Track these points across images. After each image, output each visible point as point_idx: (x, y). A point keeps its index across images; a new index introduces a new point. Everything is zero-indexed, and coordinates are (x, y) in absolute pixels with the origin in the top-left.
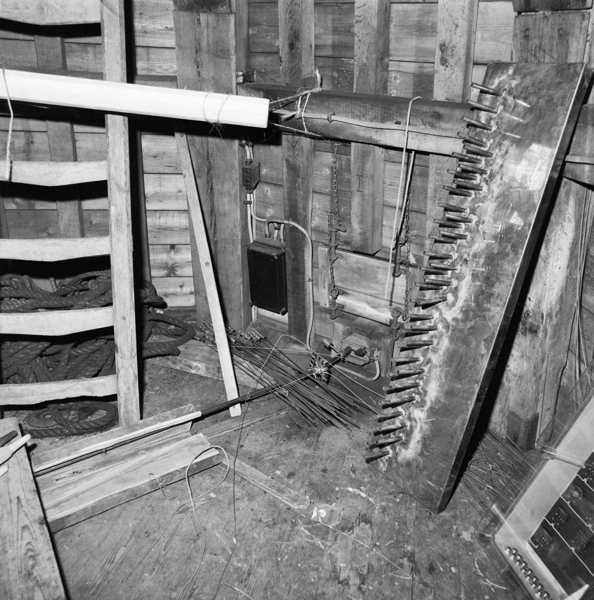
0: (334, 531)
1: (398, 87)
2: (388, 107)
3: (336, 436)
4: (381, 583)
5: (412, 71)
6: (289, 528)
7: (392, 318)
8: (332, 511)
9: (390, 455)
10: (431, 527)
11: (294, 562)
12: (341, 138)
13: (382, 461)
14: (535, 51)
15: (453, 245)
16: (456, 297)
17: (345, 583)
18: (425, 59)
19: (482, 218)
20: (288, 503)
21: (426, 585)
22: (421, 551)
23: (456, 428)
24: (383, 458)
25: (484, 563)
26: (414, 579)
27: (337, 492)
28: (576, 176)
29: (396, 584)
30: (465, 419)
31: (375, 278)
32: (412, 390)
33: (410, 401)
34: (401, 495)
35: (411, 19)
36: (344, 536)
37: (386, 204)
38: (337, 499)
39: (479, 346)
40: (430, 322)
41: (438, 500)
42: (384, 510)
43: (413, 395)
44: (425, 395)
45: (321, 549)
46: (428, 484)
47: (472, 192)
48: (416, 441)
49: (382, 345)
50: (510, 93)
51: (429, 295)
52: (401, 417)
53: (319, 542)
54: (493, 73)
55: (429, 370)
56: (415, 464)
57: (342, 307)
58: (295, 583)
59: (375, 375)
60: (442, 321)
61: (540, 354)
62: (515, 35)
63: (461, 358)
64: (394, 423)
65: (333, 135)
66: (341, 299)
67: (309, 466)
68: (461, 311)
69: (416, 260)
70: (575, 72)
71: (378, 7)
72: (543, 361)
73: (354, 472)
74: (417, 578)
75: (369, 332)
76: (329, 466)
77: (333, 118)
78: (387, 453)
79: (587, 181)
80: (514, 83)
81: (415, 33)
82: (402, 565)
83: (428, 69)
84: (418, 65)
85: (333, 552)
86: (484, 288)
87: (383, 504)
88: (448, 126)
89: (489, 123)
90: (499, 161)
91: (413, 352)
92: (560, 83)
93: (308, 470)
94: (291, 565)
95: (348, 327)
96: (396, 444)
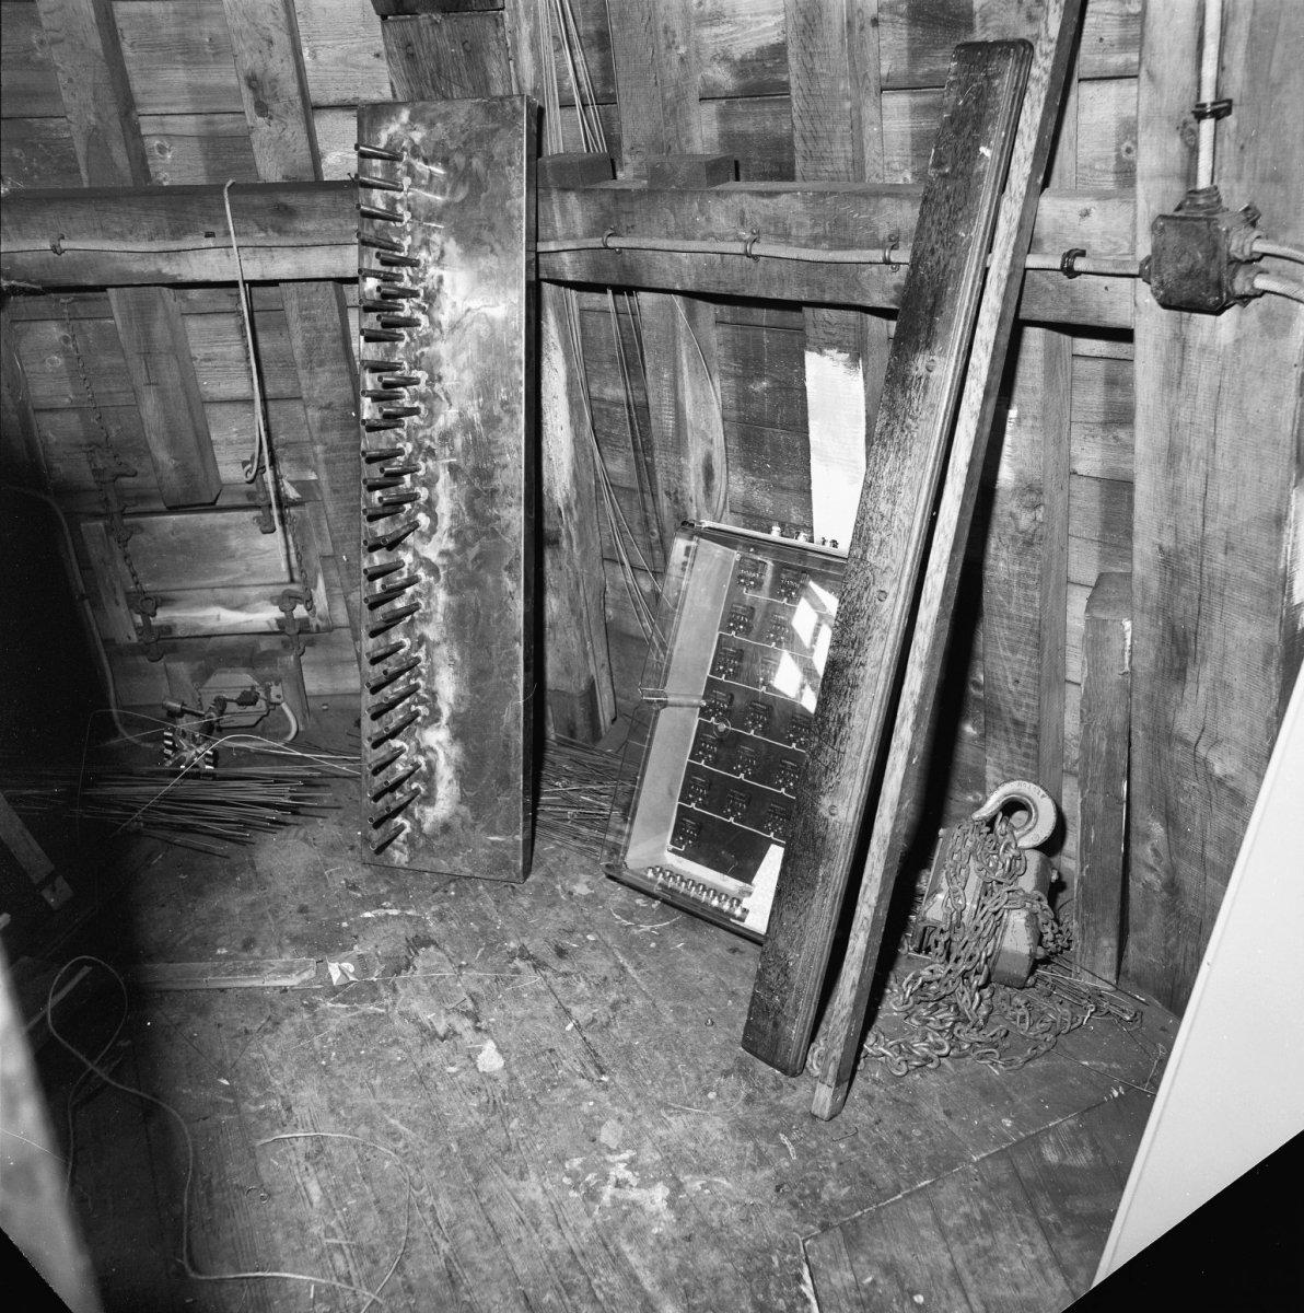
0: (385, 982)
1: (175, 165)
2: (185, 209)
3: (284, 853)
4: (503, 1007)
5: (193, 131)
6: (306, 1016)
7: (282, 615)
8: (361, 957)
9: (408, 830)
10: (526, 903)
11: (352, 1054)
12: (91, 283)
13: (396, 848)
14: (432, 80)
15: (398, 430)
16: (434, 517)
17: (451, 1034)
18: (215, 107)
19: (436, 372)
20: (278, 983)
21: (566, 974)
22: (531, 939)
23: (507, 728)
24: (395, 842)
25: (625, 908)
26: (545, 977)
27: (348, 929)
28: (555, 273)
29: (525, 995)
30: (518, 705)
31: (225, 549)
32: (407, 700)
33: (409, 723)
34: (453, 885)
35: (164, 31)
36: (405, 981)
37: (207, 399)
38: (356, 937)
39: (501, 582)
40: (401, 574)
41: (516, 858)
42: (441, 917)
43: (413, 708)
44: (435, 699)
45: (381, 1015)
46: (493, 842)
47: (402, 331)
48: (446, 783)
49: (279, 671)
50: (415, 153)
51: (381, 528)
52: (403, 757)
53: (371, 1008)
54: (371, 122)
55: (428, 654)
56: (458, 821)
57: (168, 629)
58: (375, 1077)
59: (288, 733)
60: (421, 564)
61: (571, 575)
62: (389, 54)
63: (477, 615)
64: (394, 771)
65: (73, 281)
66: (162, 616)
67: (270, 917)
68: (451, 535)
69: (298, 490)
70: (514, 110)
71: (95, 10)
72: (578, 586)
73: (354, 888)
74: (548, 974)
75: (247, 655)
76: (302, 899)
77: (64, 245)
78: (402, 827)
79: (570, 277)
80: (417, 136)
81: (179, 58)
82: (517, 971)
83: (226, 124)
84: (203, 118)
85: (403, 1009)
86: (477, 485)
87: (433, 909)
88: (310, 226)
89: (394, 209)
90: (433, 271)
91: (388, 637)
92: (497, 130)
93: (272, 921)
94: (349, 1060)
95: (198, 664)
96: (410, 806)
